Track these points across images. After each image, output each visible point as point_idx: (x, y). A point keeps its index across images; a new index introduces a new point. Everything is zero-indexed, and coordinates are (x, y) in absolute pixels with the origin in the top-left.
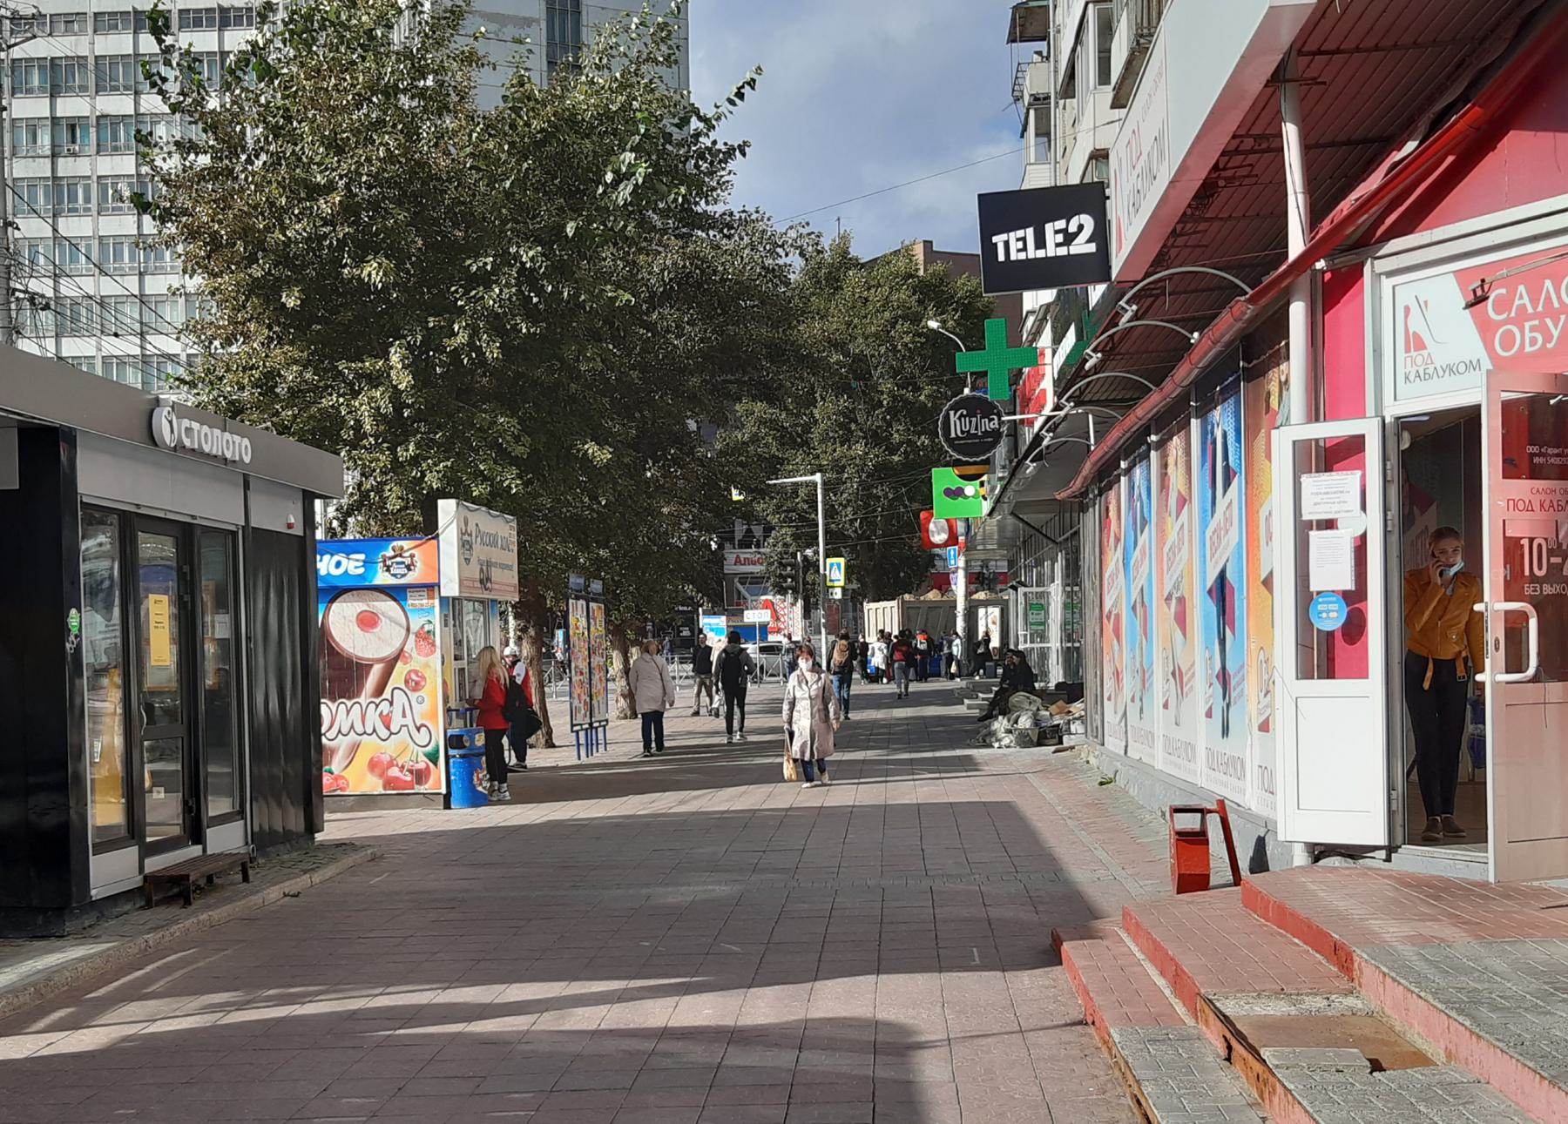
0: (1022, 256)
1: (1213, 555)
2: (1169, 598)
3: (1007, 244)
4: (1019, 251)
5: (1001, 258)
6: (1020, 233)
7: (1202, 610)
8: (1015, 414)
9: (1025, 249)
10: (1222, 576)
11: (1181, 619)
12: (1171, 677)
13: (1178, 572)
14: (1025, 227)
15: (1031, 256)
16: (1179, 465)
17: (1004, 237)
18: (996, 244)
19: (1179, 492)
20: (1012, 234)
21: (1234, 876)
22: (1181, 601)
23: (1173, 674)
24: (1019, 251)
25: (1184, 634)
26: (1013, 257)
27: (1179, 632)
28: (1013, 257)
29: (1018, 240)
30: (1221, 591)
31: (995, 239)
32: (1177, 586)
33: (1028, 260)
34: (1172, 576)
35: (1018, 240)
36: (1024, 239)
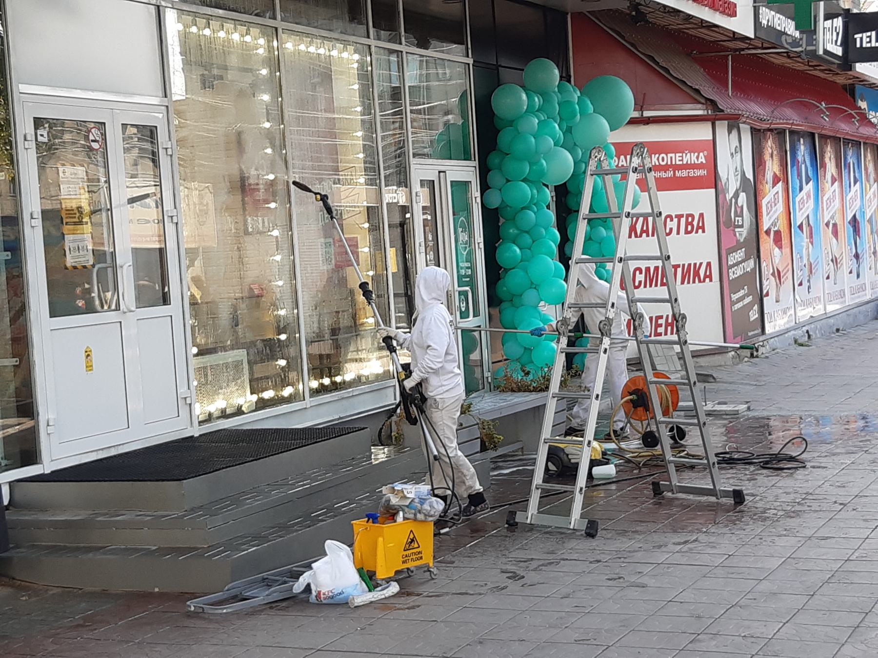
0: (869, 45)
1: (827, 209)
2: (827, 225)
3: (861, 39)
4: (867, 42)
5: (858, 45)
6: (869, 34)
7: (846, 231)
8: (428, 108)
9: (870, 42)
10: (854, 216)
11: (835, 233)
12: (831, 263)
13: (775, 216)
14: (871, 30)
15: (873, 45)
16: (774, 157)
17: (860, 35)
18: (856, 39)
19: (775, 173)
20: (864, 34)
21: (405, 412)
22: (835, 225)
23: (832, 260)
24: (867, 42)
25: (837, 239)
26: (864, 45)
27: (834, 239)
28: (864, 45)
29: (867, 37)
30: (854, 222)
31: (856, 36)
32: (832, 217)
33: (871, 48)
34: (803, 213)
35: (867, 37)
36: (870, 37)
